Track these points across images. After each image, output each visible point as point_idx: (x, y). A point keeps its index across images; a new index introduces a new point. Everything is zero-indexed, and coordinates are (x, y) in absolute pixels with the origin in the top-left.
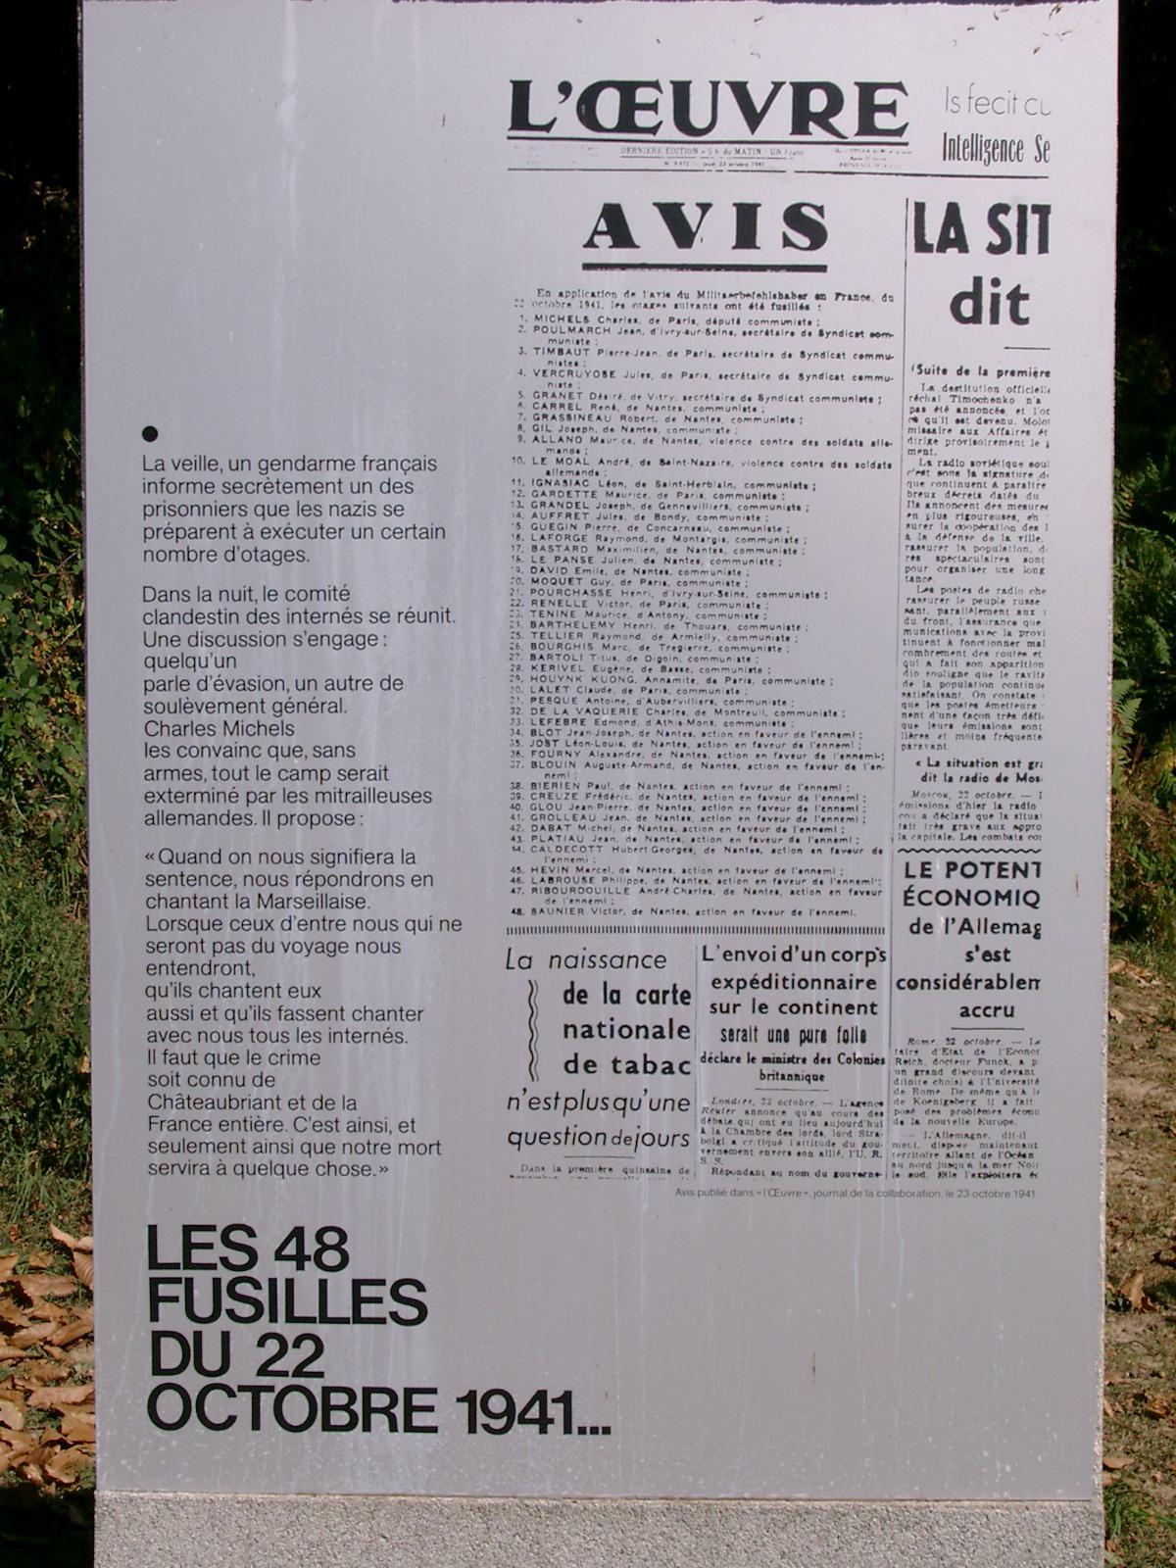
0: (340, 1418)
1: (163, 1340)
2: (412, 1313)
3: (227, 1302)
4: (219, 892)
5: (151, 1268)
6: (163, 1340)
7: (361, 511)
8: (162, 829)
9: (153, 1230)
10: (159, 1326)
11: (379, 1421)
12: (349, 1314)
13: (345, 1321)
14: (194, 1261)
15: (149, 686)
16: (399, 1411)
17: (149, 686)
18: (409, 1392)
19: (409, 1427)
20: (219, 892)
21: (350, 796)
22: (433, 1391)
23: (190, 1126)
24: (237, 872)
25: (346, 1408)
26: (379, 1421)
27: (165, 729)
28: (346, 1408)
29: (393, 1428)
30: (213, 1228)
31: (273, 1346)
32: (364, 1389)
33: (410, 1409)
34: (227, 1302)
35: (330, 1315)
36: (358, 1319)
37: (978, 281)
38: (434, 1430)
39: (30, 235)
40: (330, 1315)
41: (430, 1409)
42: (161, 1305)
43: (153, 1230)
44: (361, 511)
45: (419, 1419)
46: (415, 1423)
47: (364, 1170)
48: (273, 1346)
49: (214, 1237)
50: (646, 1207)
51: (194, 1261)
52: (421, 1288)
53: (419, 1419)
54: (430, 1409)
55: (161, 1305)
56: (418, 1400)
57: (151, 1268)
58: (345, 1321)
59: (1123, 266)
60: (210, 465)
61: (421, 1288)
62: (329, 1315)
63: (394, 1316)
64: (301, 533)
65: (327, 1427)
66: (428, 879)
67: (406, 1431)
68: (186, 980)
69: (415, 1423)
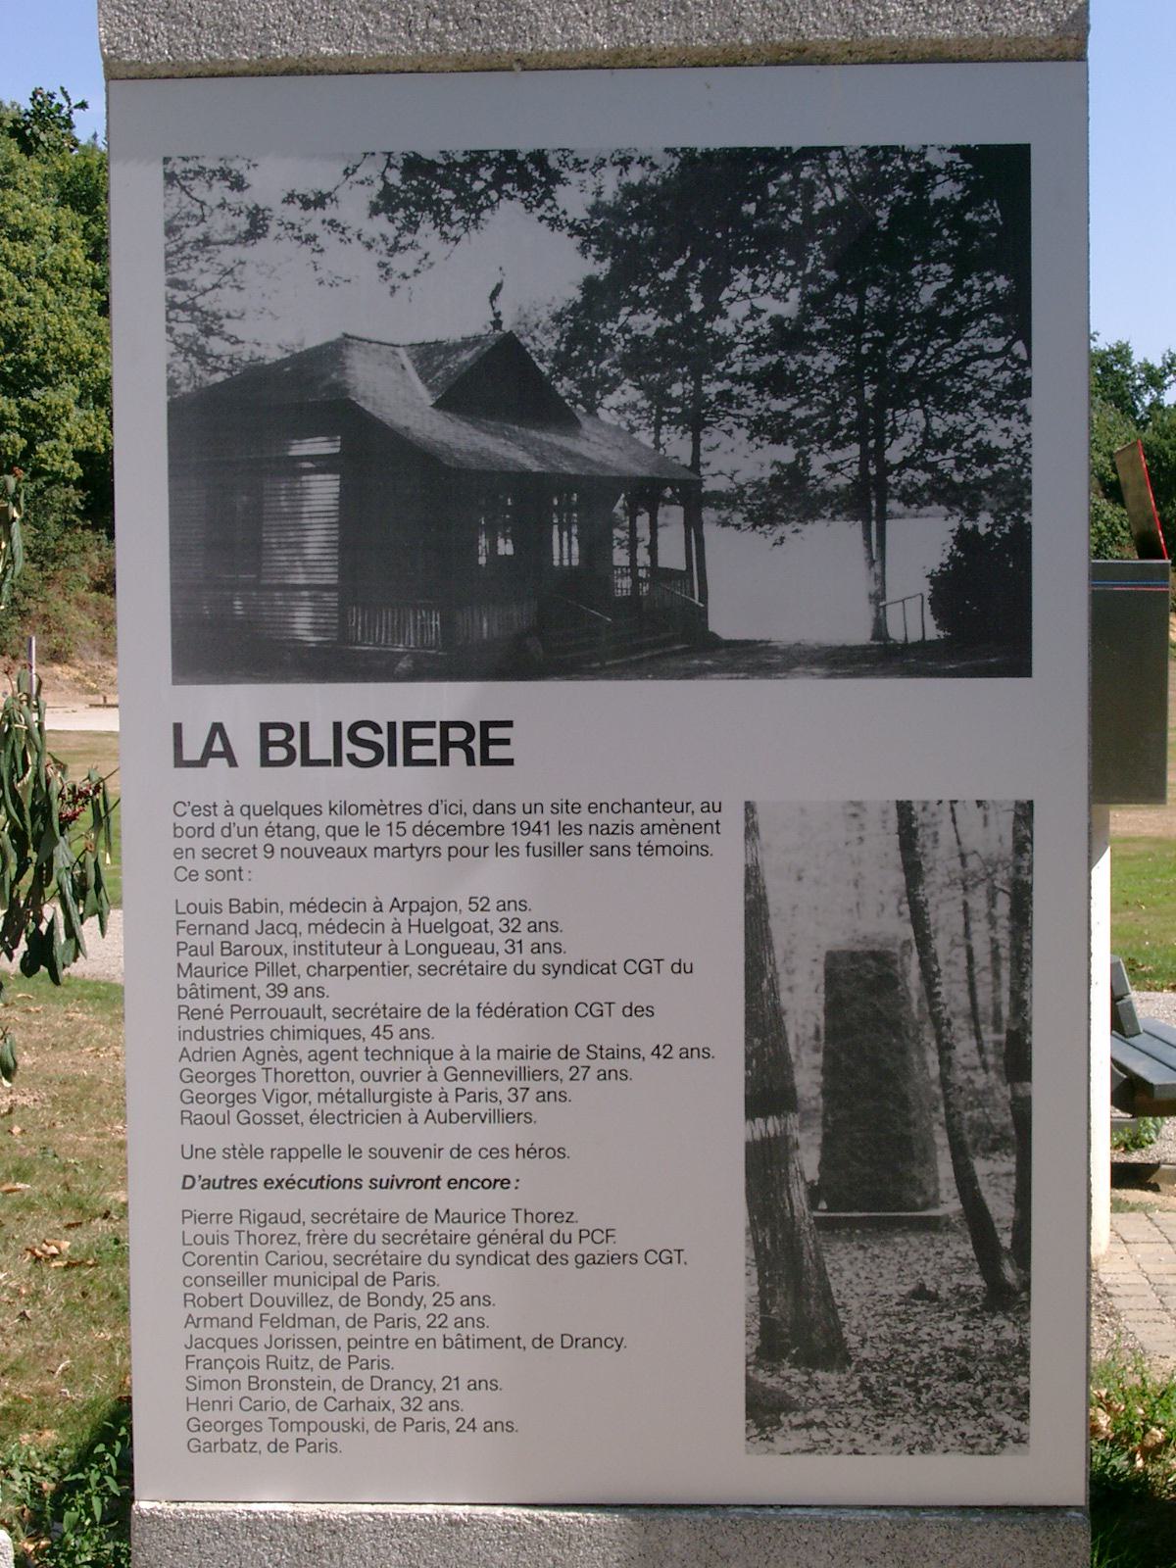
0: (277, 753)
3: (348, 747)
4: (350, 1045)
5: (405, 723)
7: (619, 830)
9: (178, 728)
11: (457, 755)
13: (325, 763)
16: (475, 745)
18: (485, 726)
19: (486, 761)
20: (350, 1045)
22: (509, 724)
25: (283, 744)
26: (457, 755)
28: (283, 744)
29: (470, 762)
30: (431, 725)
31: (574, 1070)
33: (486, 742)
34: (348, 747)
35: (312, 757)
38: (509, 762)
41: (506, 742)
43: (178, 728)
44: (619, 830)
45: (495, 752)
46: (492, 756)
48: (574, 1070)
53: (495, 752)
54: (506, 742)
56: (494, 733)
57: (405, 723)
58: (325, 763)
60: (596, 852)
64: (302, 1184)
65: (409, 761)
67: (405, 764)
69: (492, 756)
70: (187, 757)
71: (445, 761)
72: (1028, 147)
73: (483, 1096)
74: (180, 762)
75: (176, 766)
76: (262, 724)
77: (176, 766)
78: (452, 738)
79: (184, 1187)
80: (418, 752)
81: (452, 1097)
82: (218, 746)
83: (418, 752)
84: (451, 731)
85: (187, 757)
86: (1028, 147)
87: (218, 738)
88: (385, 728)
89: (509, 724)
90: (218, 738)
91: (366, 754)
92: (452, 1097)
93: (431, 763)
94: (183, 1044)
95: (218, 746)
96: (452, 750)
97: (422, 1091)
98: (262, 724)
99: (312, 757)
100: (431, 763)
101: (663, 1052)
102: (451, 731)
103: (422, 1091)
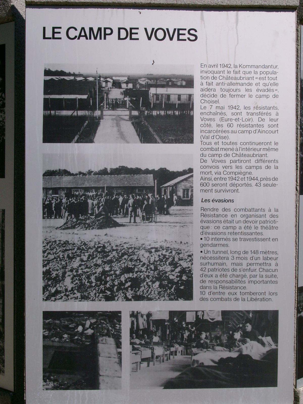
2: (193, 38)
5: (104, 28)
6: (121, 30)
9: (44, 28)
12: (51, 36)
13: (50, 38)
14: (133, 38)
15: (231, 161)
17: (231, 161)
21: (268, 264)
27: (237, 155)
30: (185, 29)
32: (130, 28)
35: (46, 37)
36: (54, 38)
37: (105, 38)
38: (60, 38)
39: (206, 332)
40: (46, 37)
41: (137, 33)
42: (107, 36)
43: (44, 28)
45: (134, 36)
46: (55, 37)
49: (186, 32)
51: (133, 38)
52: (196, 31)
53: (134, 36)
55: (107, 36)
56: (133, 31)
57: (104, 28)
58: (50, 38)
61: (196, 31)
63: (189, 39)
66: (236, 216)
70: (121, 37)
74: (44, 38)
75: (44, 39)
76: (53, 27)
77: (44, 39)
78: (107, 33)
79: (44, 38)
82: (83, 34)
84: (107, 30)
85: (121, 37)
89: (138, 29)
94: (202, 175)
95: (83, 34)
97: (224, 268)
98: (53, 27)
101: (203, 270)
102: (107, 30)
103: (224, 268)
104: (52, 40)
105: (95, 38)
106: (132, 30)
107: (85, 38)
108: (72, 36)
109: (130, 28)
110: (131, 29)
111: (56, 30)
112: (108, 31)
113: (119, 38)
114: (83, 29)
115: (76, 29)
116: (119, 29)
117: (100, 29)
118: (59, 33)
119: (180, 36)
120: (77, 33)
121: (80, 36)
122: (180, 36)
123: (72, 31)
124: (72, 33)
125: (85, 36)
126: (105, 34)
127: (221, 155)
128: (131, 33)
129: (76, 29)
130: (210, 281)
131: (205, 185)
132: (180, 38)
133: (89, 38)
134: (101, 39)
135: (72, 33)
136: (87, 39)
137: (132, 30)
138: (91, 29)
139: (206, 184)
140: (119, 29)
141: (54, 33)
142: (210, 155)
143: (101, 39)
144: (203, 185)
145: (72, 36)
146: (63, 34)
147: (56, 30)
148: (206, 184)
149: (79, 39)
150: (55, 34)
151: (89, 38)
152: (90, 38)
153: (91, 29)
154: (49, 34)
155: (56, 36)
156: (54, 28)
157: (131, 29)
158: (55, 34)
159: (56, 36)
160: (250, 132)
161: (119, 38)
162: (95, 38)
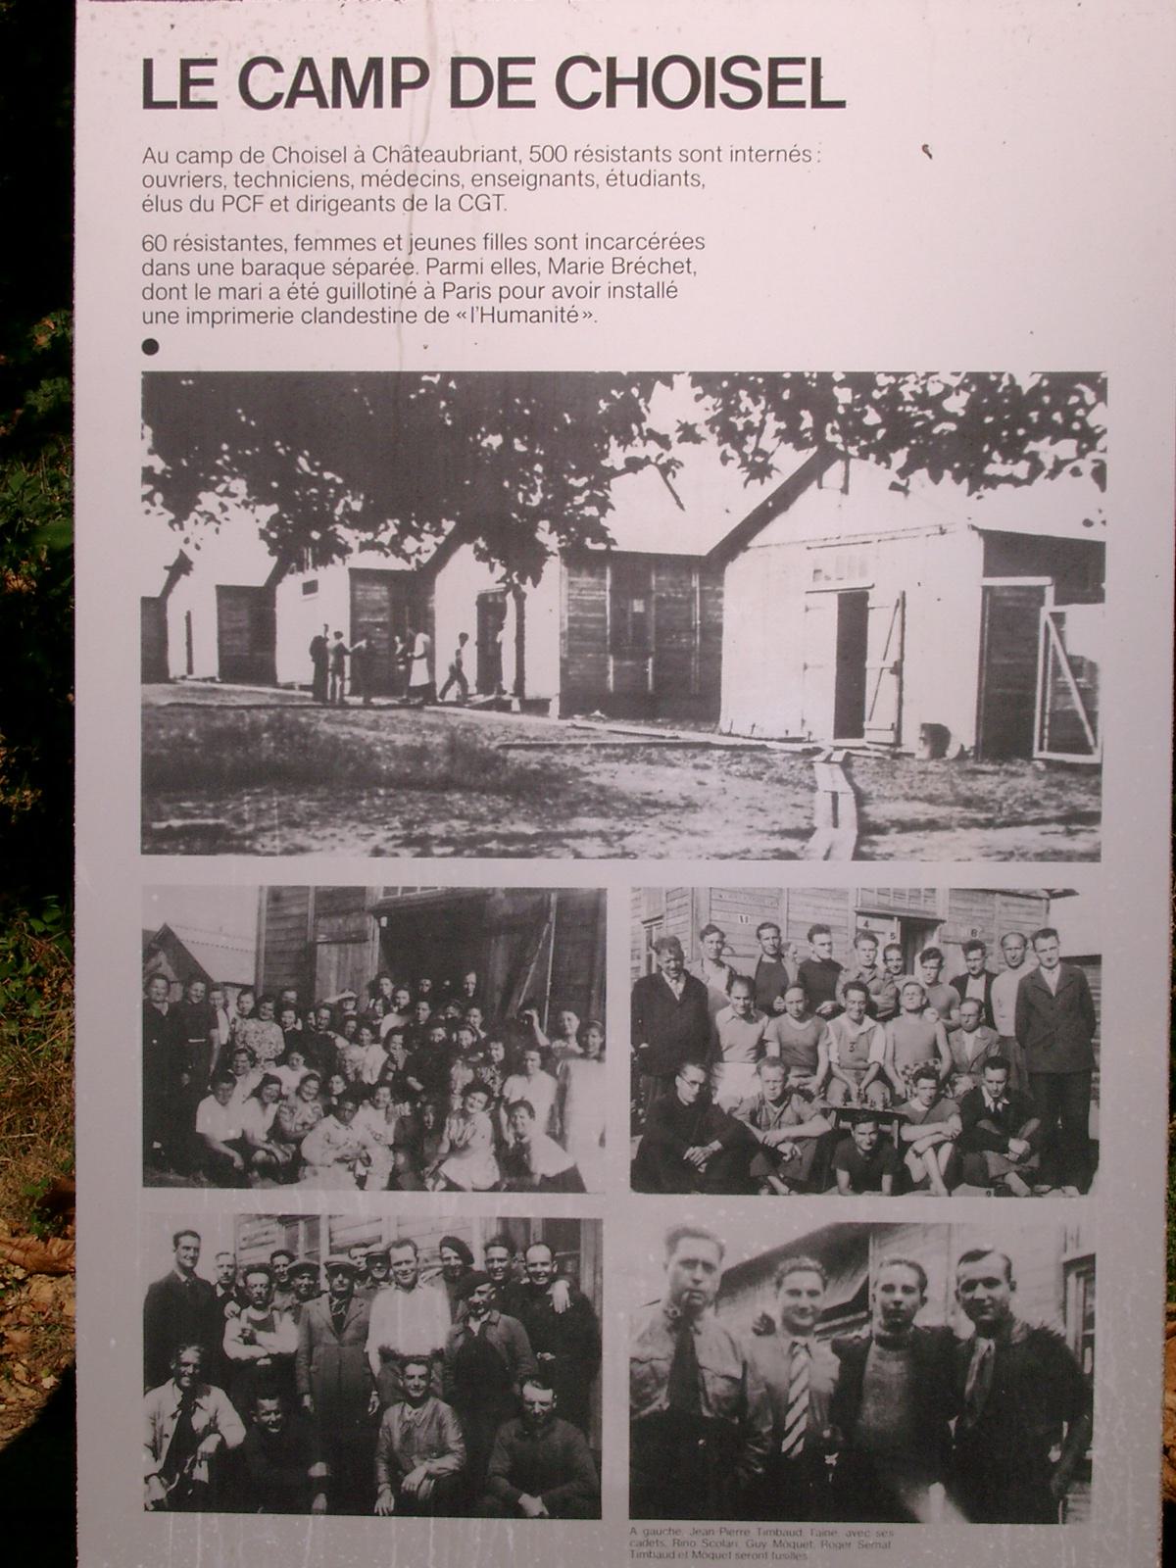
1: (464, 67)
6: (464, 67)
8: (156, 216)
9: (148, 64)
10: (809, 104)
12: (177, 98)
13: (171, 105)
14: (780, 98)
22: (530, 61)
23: (525, 292)
24: (354, 172)
27: (395, 154)
30: (801, 61)
32: (500, 59)
35: (824, 98)
36: (186, 103)
37: (396, 102)
38: (531, 104)
40: (155, 98)
41: (527, 81)
42: (636, 75)
43: (148, 64)
45: (515, 93)
47: (572, 316)
50: (432, 1118)
51: (780, 98)
53: (515, 93)
55: (636, 75)
56: (514, 71)
58: (171, 105)
59: (68, 103)
62: (463, 98)
68: (387, 193)
71: (611, 102)
72: (599, 1517)
73: (474, 291)
74: (149, 103)
79: (149, 103)
80: (785, 93)
81: (439, 293)
82: (307, 84)
83: (785, 93)
86: (599, 1517)
87: (307, 72)
88: (604, 66)
90: (307, 72)
91: (742, 94)
92: (439, 293)
93: (801, 104)
95: (307, 84)
96: (619, 88)
99: (463, 98)
100: (801, 104)
104: (179, 111)
105: (357, 102)
106: (780, 67)
107: (315, 99)
108: (260, 94)
109: (500, 59)
110: (504, 63)
111: (196, 72)
112: (410, 73)
113: (457, 102)
114: (307, 63)
115: (277, 67)
116: (457, 63)
117: (375, 64)
118: (527, 81)
119: (193, 89)
120: (284, 83)
121: (296, 92)
122: (193, 89)
123: (261, 71)
124: (264, 83)
125: (317, 92)
126: (398, 86)
127: (227, 157)
128: (505, 82)
129: (277, 67)
130: (580, 154)
131: (548, 154)
132: (511, 97)
133: (330, 103)
134: (378, 103)
135: (264, 83)
136: (323, 104)
137: (780, 67)
138: (340, 66)
139: (554, 154)
140: (457, 63)
141: (186, 83)
142: (182, 157)
143: (378, 103)
144: (542, 156)
145: (260, 94)
146: (543, 89)
147: (196, 72)
148: (554, 154)
149: (290, 104)
150: (780, 87)
151: (330, 103)
152: (337, 103)
153: (340, 66)
154: (167, 86)
155: (197, 93)
156: (186, 65)
157: (504, 63)
158: (781, 88)
159: (197, 93)
160: (227, 157)
161: (457, 102)
162: (357, 102)
